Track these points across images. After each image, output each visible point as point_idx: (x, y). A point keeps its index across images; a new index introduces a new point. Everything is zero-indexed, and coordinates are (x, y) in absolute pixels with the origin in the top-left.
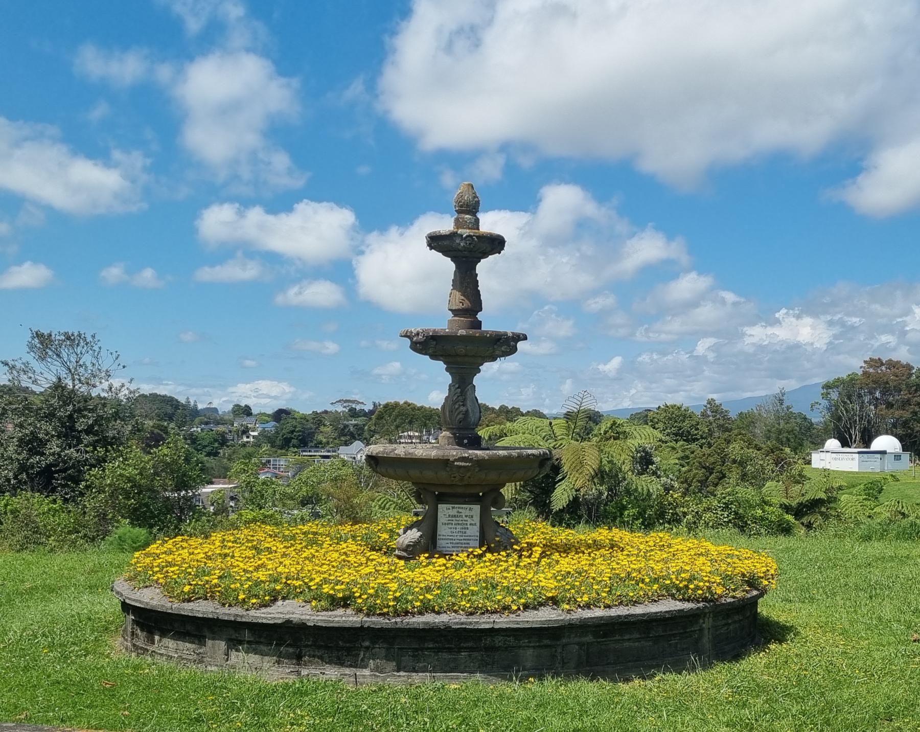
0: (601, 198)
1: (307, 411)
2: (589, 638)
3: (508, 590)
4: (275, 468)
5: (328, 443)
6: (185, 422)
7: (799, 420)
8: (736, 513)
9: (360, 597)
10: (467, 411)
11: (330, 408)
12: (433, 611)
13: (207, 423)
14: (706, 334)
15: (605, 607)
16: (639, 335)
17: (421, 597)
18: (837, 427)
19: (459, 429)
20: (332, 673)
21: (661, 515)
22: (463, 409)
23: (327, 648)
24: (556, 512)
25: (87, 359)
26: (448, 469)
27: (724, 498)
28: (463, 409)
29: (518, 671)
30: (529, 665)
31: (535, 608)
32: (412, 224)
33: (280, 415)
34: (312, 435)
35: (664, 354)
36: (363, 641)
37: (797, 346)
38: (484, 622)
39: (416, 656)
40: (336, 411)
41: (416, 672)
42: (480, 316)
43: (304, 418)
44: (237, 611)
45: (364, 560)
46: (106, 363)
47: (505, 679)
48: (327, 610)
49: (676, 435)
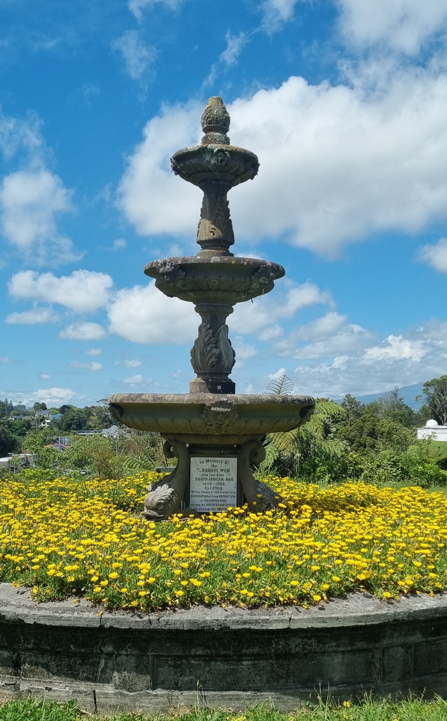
2: (417, 638)
3: (303, 571)
4: (62, 443)
5: (95, 427)
6: (5, 414)
8: (402, 469)
9: (98, 582)
10: (220, 354)
11: (96, 405)
12: (202, 602)
13: (18, 415)
14: (342, 353)
15: (435, 593)
17: (184, 583)
18: (433, 412)
19: (211, 374)
21: (345, 470)
22: (215, 351)
23: (53, 653)
26: (203, 416)
27: (393, 457)
28: (215, 351)
29: (324, 686)
30: (337, 677)
31: (342, 596)
33: (64, 409)
36: (104, 644)
39: (179, 666)
40: (100, 406)
41: (180, 689)
43: (80, 411)
45: (108, 521)
47: (306, 699)
48: (52, 599)
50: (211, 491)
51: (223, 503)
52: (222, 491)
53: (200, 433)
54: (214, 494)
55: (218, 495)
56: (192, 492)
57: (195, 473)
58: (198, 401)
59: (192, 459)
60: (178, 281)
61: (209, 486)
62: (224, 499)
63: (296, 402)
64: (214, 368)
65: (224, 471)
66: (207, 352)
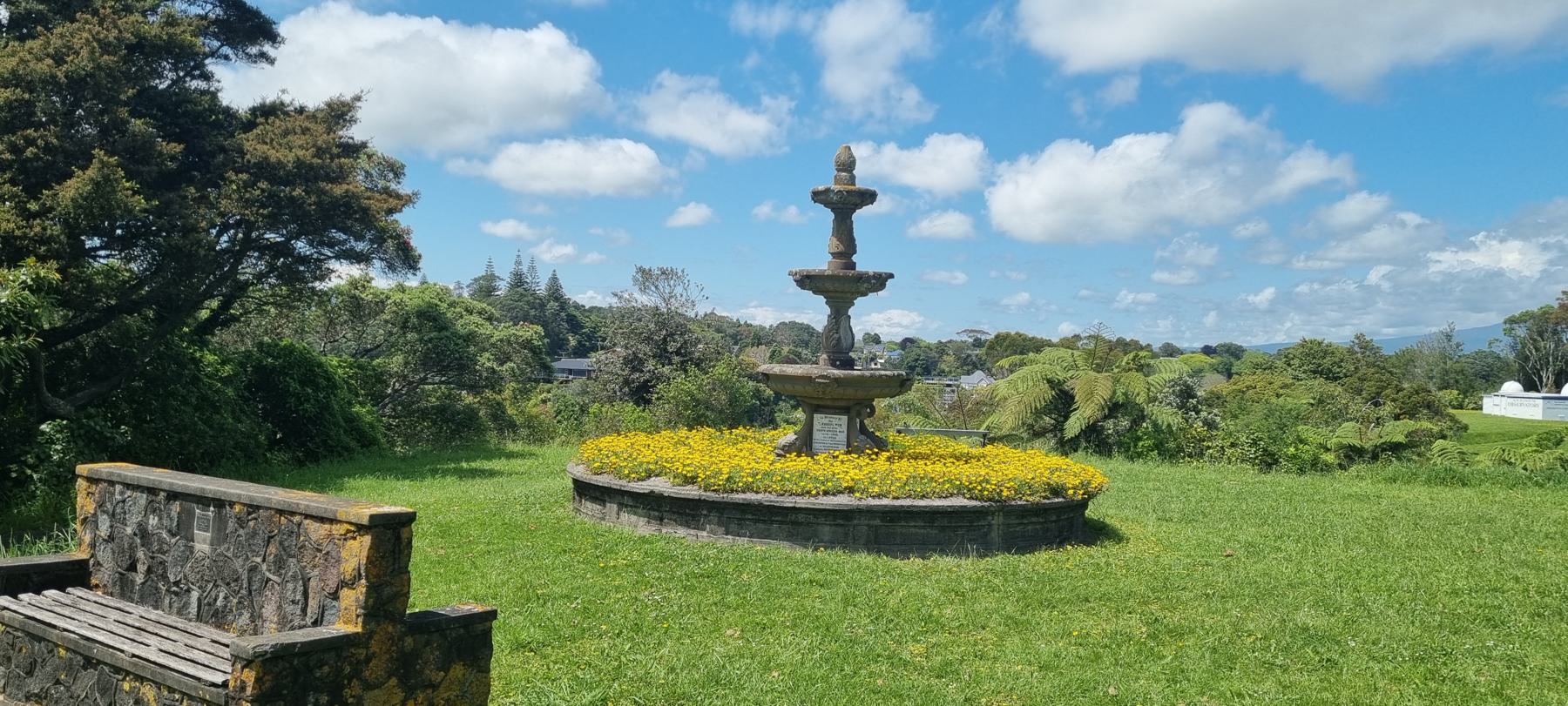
0: (1249, 112)
1: (932, 340)
7: (1490, 360)
14: (1379, 261)
16: (1299, 264)
20: (682, 532)
25: (678, 290)
32: (1042, 151)
33: (907, 343)
34: (935, 363)
35: (1325, 283)
37: (1500, 274)
38: (788, 502)
42: (854, 258)
43: (929, 347)
44: (623, 482)
46: (694, 294)
49: (1314, 372)
57: (816, 426)
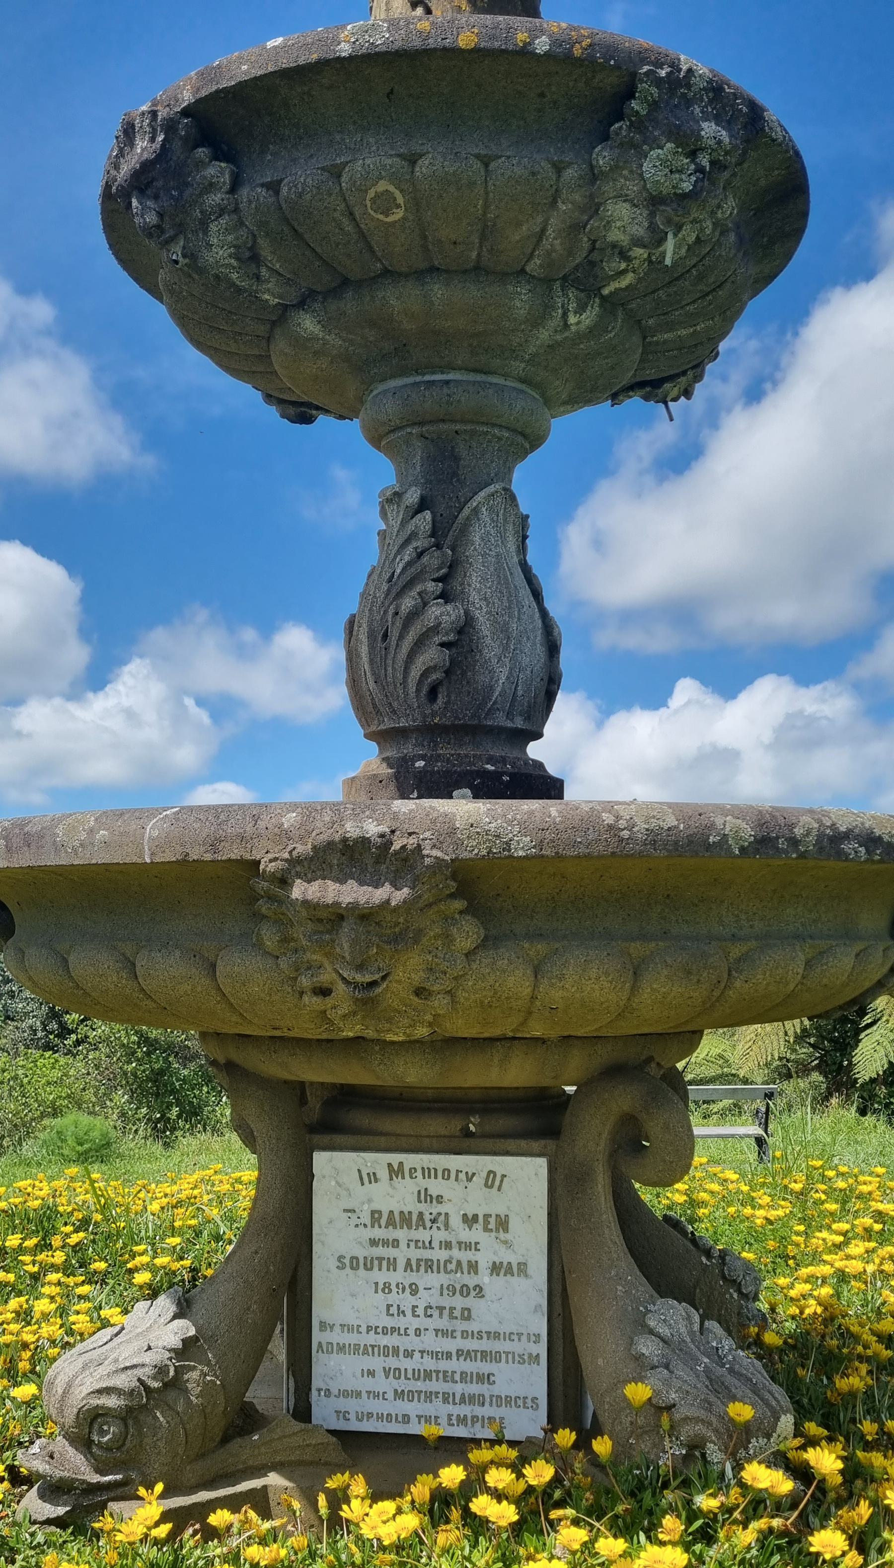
10: (465, 628)
19: (430, 732)
22: (442, 614)
24: (862, 1085)
28: (442, 614)
50: (415, 1323)
51: (474, 1388)
52: (473, 1326)
53: (291, 1034)
54: (430, 1342)
55: (450, 1345)
56: (323, 1326)
57: (335, 1233)
58: (214, 845)
59: (321, 1160)
60: (204, 225)
61: (407, 1301)
62: (485, 1368)
63: (848, 847)
64: (441, 700)
65: (479, 1226)
66: (399, 624)
